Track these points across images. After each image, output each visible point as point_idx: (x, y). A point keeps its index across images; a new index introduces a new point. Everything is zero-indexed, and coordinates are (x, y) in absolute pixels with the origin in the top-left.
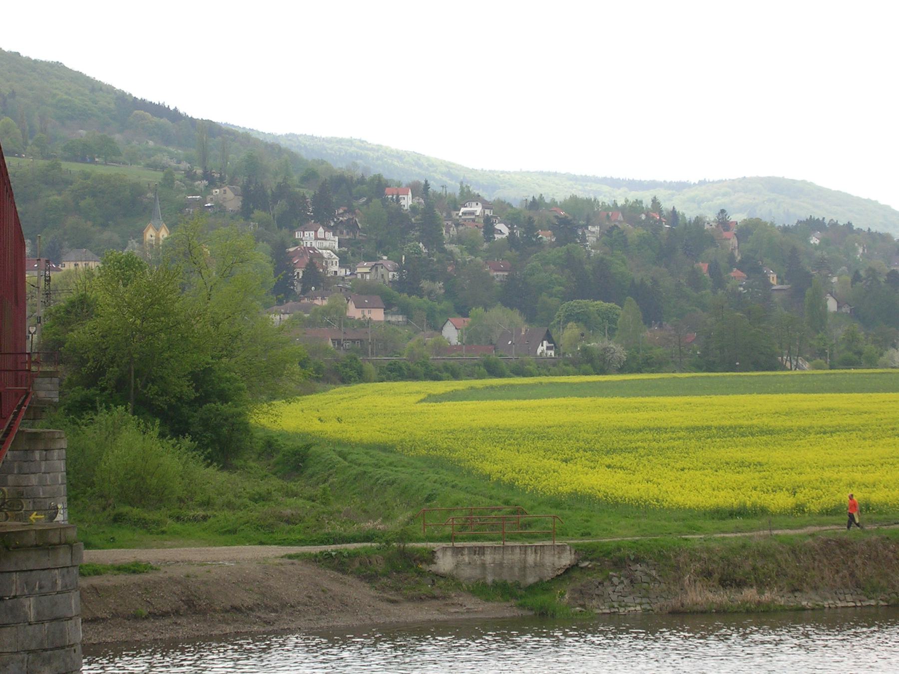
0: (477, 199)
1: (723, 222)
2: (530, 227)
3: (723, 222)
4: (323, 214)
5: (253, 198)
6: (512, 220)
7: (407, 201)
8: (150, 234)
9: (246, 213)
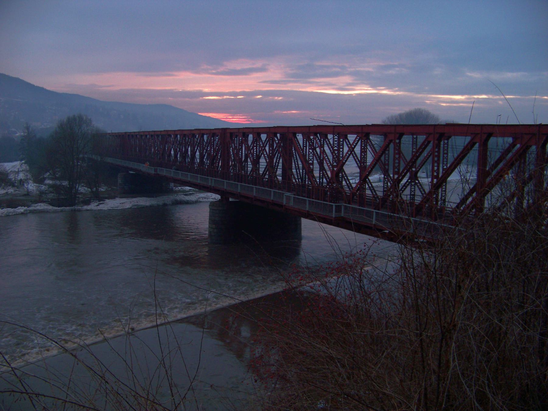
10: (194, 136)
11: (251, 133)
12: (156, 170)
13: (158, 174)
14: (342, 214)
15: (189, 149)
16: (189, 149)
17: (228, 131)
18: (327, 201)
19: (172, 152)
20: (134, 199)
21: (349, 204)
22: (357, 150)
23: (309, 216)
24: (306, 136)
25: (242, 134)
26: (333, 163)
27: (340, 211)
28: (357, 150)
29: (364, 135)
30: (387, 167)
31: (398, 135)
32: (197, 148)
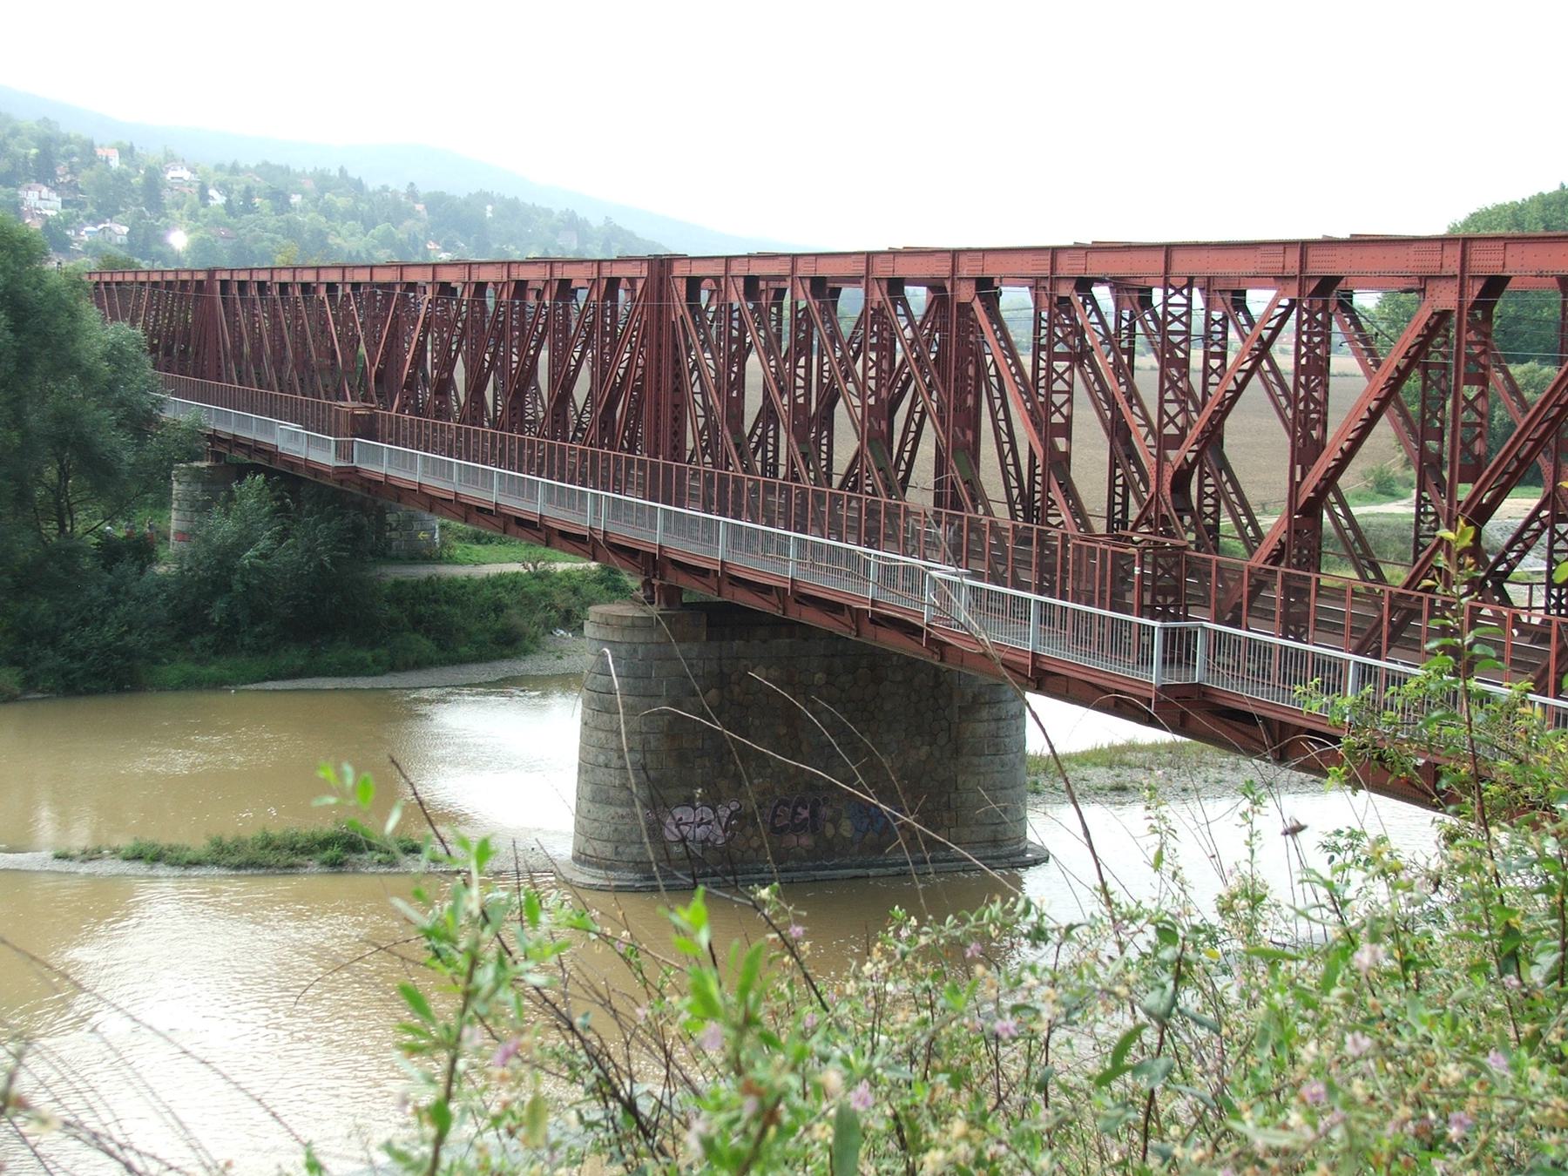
1: (412, 194)
3: (412, 194)
6: (223, 187)
10: (825, 290)
11: (853, 280)
12: (343, 451)
13: (356, 470)
14: (1198, 675)
15: (544, 355)
16: (544, 355)
17: (679, 270)
18: (1126, 610)
19: (459, 374)
20: (865, 593)
21: (1235, 623)
22: (1284, 356)
23: (1046, 679)
24: (1134, 294)
25: (741, 283)
26: (1161, 425)
27: (1187, 659)
28: (1284, 356)
29: (1312, 286)
30: (1061, 443)
31: (1478, 287)
32: (583, 354)
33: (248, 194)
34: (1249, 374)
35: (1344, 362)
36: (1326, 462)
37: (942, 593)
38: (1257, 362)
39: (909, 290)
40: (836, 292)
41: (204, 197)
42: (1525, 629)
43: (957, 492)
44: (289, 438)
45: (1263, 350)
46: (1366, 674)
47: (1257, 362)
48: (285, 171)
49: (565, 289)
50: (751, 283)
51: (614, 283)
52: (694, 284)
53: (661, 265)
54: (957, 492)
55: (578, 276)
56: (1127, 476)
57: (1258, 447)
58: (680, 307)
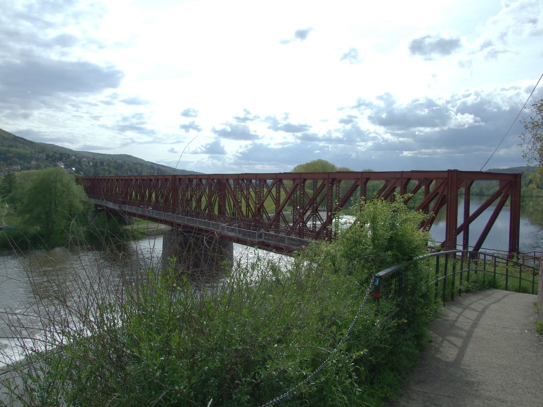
0: (85, 157)
2: (97, 163)
4: (60, 159)
5: (48, 157)
6: (92, 161)
7: (73, 157)
8: (32, 163)
9: (47, 159)
12: (120, 207)
14: (263, 240)
17: (177, 177)
19: (133, 193)
23: (239, 241)
33: (97, 163)
34: (268, 195)
35: (283, 193)
36: (280, 208)
37: (222, 228)
38: (269, 193)
39: (285, 182)
40: (192, 180)
41: (89, 163)
42: (310, 231)
43: (222, 211)
44: (111, 205)
45: (270, 192)
46: (289, 239)
47: (269, 193)
48: (185, 111)
49: (151, 180)
50: (189, 179)
51: (158, 179)
52: (180, 179)
53: (175, 176)
54: (222, 211)
55: (152, 178)
56: (249, 209)
57: (270, 206)
58: (178, 183)
